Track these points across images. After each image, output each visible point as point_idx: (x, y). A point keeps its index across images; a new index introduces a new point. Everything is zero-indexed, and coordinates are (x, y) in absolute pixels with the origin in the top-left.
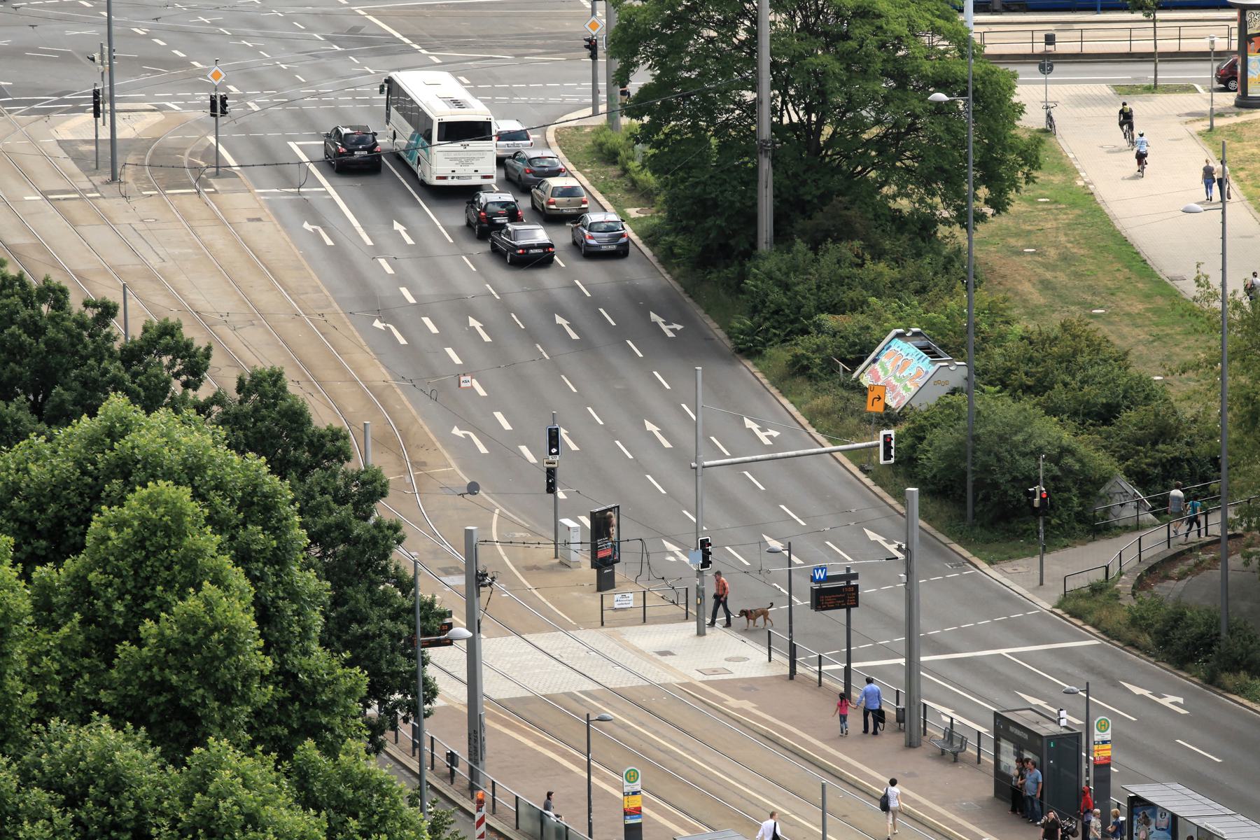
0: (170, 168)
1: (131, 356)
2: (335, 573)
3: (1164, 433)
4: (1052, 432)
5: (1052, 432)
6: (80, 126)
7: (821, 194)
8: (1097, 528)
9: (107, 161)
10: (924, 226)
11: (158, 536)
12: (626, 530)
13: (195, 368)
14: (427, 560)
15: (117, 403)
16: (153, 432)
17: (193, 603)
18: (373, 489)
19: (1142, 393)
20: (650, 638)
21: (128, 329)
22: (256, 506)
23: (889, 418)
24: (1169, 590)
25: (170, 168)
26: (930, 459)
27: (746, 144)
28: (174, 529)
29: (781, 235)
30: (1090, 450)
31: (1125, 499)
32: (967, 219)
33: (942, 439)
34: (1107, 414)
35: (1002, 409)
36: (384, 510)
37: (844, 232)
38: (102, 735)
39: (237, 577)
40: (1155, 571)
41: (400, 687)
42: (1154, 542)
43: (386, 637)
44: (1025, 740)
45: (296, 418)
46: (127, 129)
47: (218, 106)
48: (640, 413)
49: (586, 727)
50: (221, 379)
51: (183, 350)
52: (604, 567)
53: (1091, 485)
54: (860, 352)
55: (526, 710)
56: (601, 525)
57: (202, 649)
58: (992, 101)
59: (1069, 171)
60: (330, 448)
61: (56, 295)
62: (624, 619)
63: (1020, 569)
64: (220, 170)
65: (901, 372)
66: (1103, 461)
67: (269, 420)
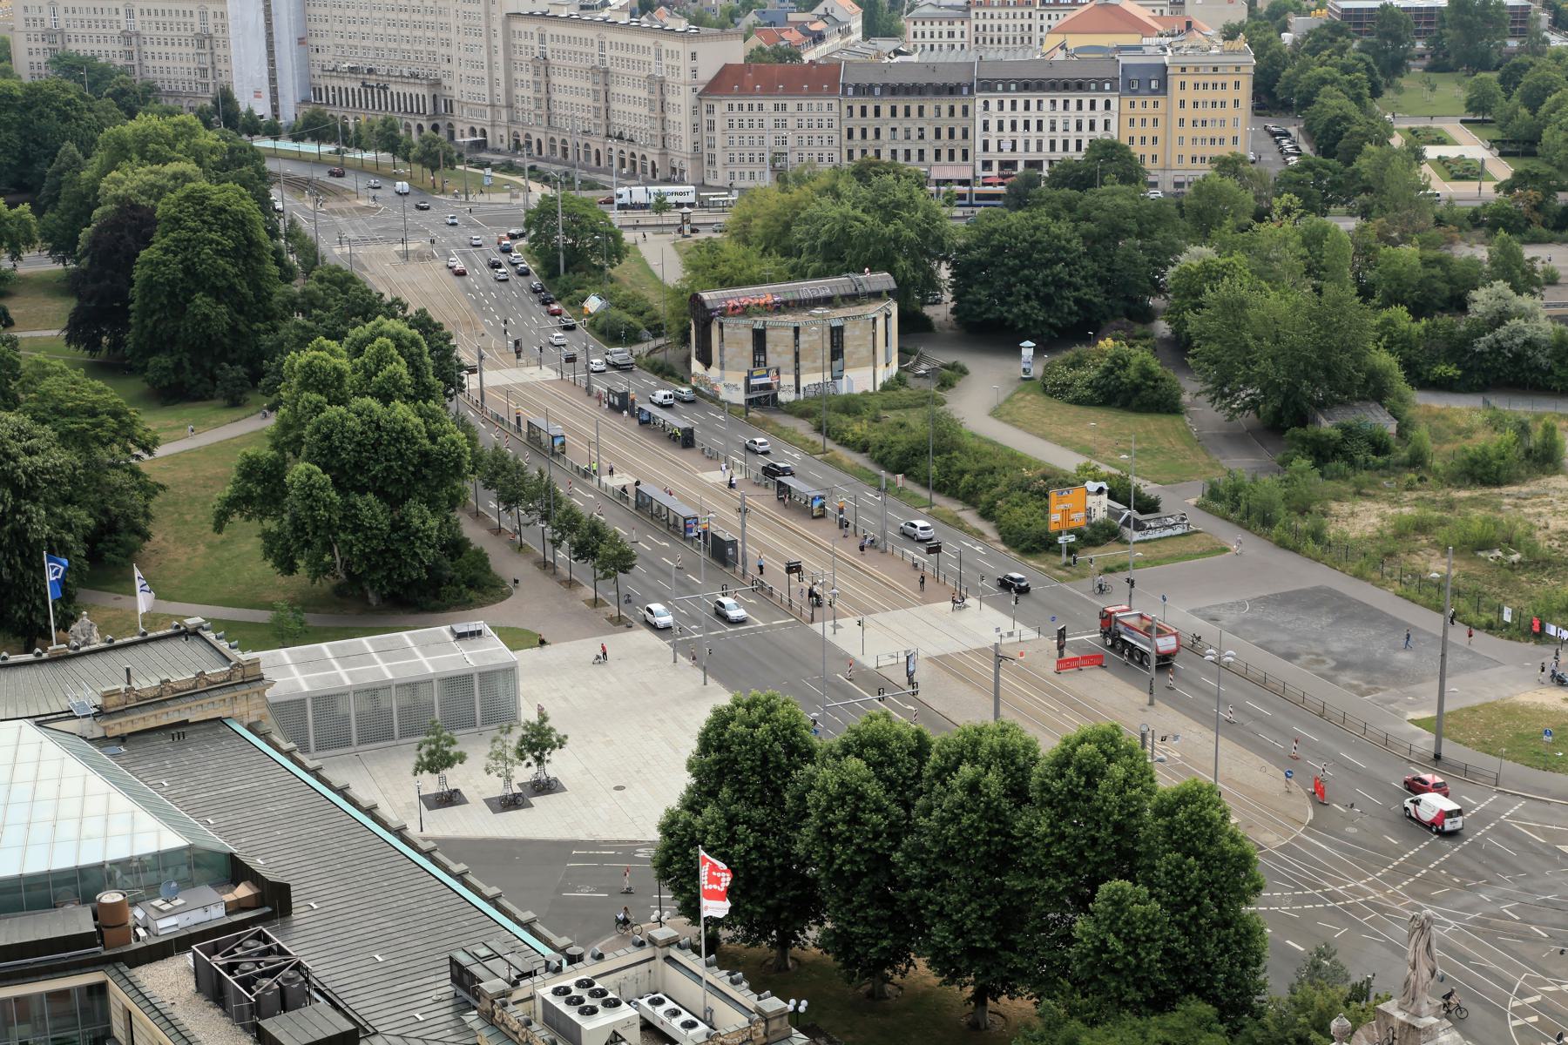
0: (421, 257)
1: (389, 305)
2: (438, 359)
3: (655, 318)
4: (630, 318)
5: (630, 318)
6: (399, 247)
7: (576, 259)
8: (639, 341)
9: (406, 255)
10: (602, 268)
11: (382, 350)
12: (524, 345)
13: (405, 308)
14: (466, 356)
15: (380, 317)
16: (392, 325)
17: (390, 367)
18: (449, 337)
19: (650, 308)
20: (528, 370)
21: (388, 298)
22: (415, 342)
23: (590, 315)
24: (654, 356)
25: (421, 257)
26: (598, 325)
27: (556, 249)
28: (387, 347)
29: (566, 271)
30: (637, 323)
31: (645, 334)
32: (612, 266)
33: (601, 320)
34: (641, 313)
35: (615, 313)
36: (453, 342)
37: (580, 270)
38: (368, 400)
39: (402, 360)
40: (652, 352)
41: (452, 382)
42: (652, 345)
43: (450, 374)
44: (616, 394)
45: (430, 320)
46: (411, 247)
47: (433, 242)
48: (530, 314)
49: (507, 391)
50: (411, 311)
51: (401, 304)
52: (518, 353)
53: (637, 331)
54: (584, 299)
55: (497, 388)
56: (517, 343)
57: (393, 379)
58: (617, 237)
59: (639, 253)
60: (439, 327)
61: (369, 292)
62: (522, 366)
63: (1409, 252)
64: (434, 257)
65: (593, 304)
66: (640, 325)
67: (423, 323)
